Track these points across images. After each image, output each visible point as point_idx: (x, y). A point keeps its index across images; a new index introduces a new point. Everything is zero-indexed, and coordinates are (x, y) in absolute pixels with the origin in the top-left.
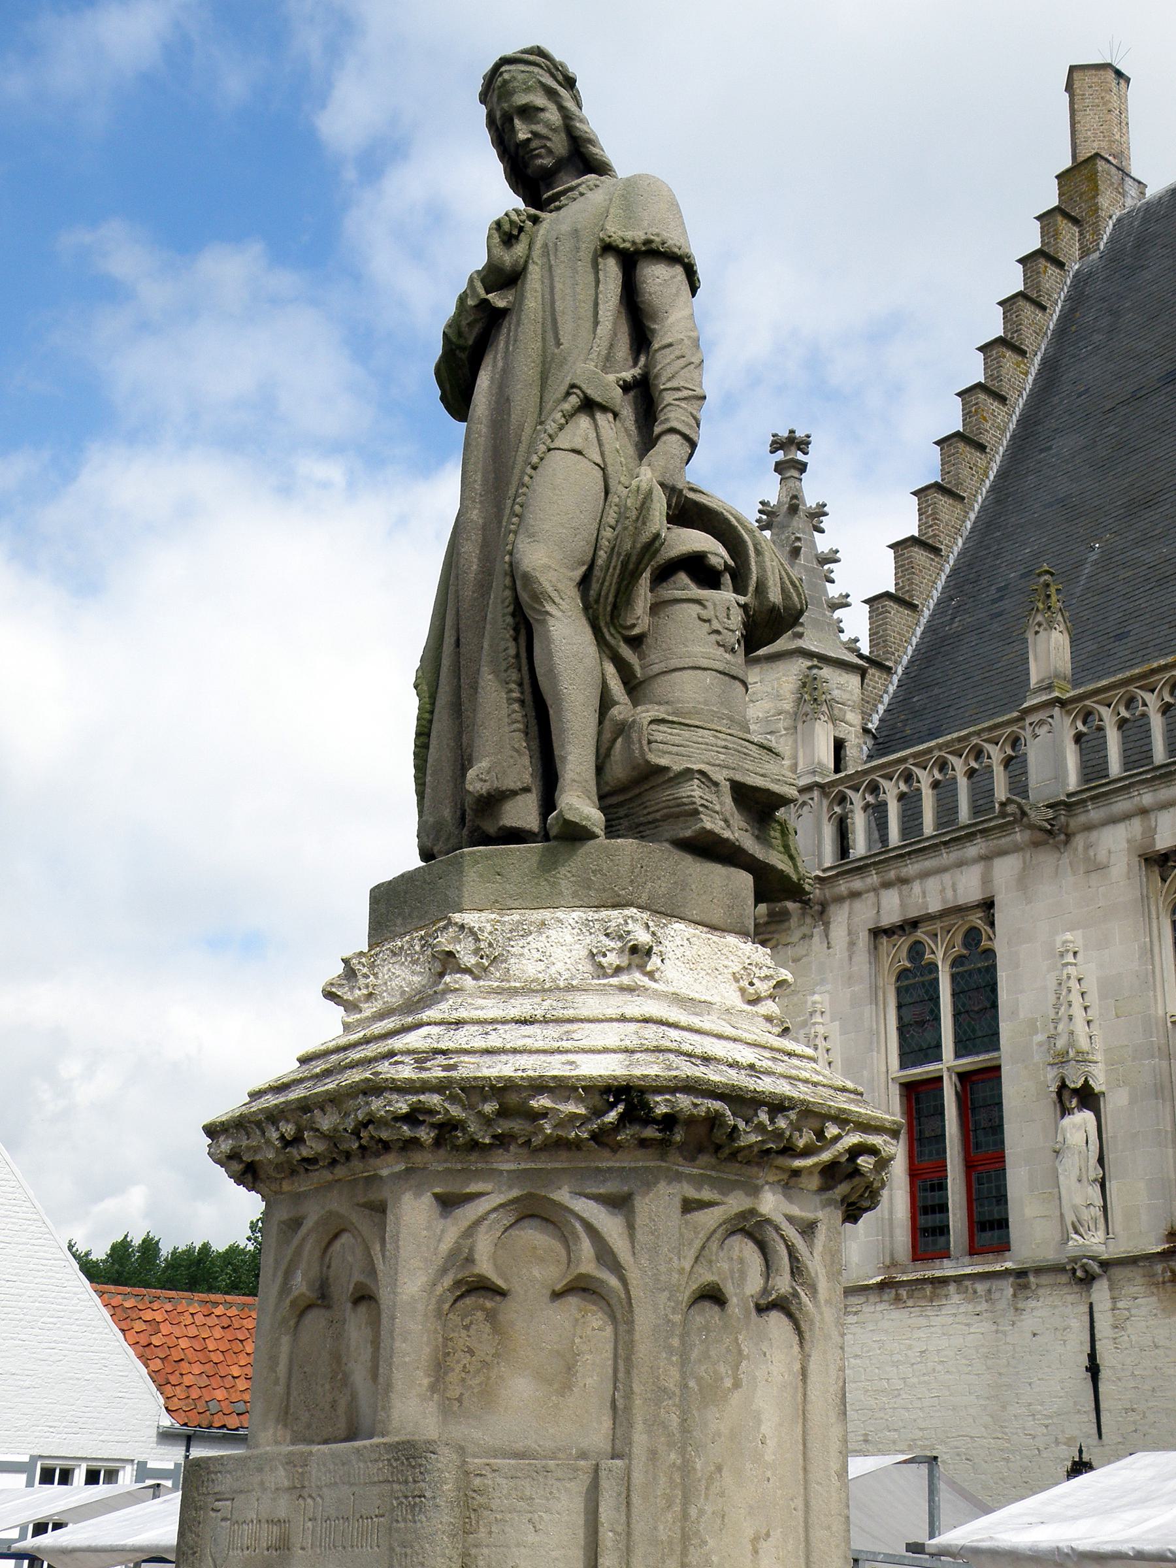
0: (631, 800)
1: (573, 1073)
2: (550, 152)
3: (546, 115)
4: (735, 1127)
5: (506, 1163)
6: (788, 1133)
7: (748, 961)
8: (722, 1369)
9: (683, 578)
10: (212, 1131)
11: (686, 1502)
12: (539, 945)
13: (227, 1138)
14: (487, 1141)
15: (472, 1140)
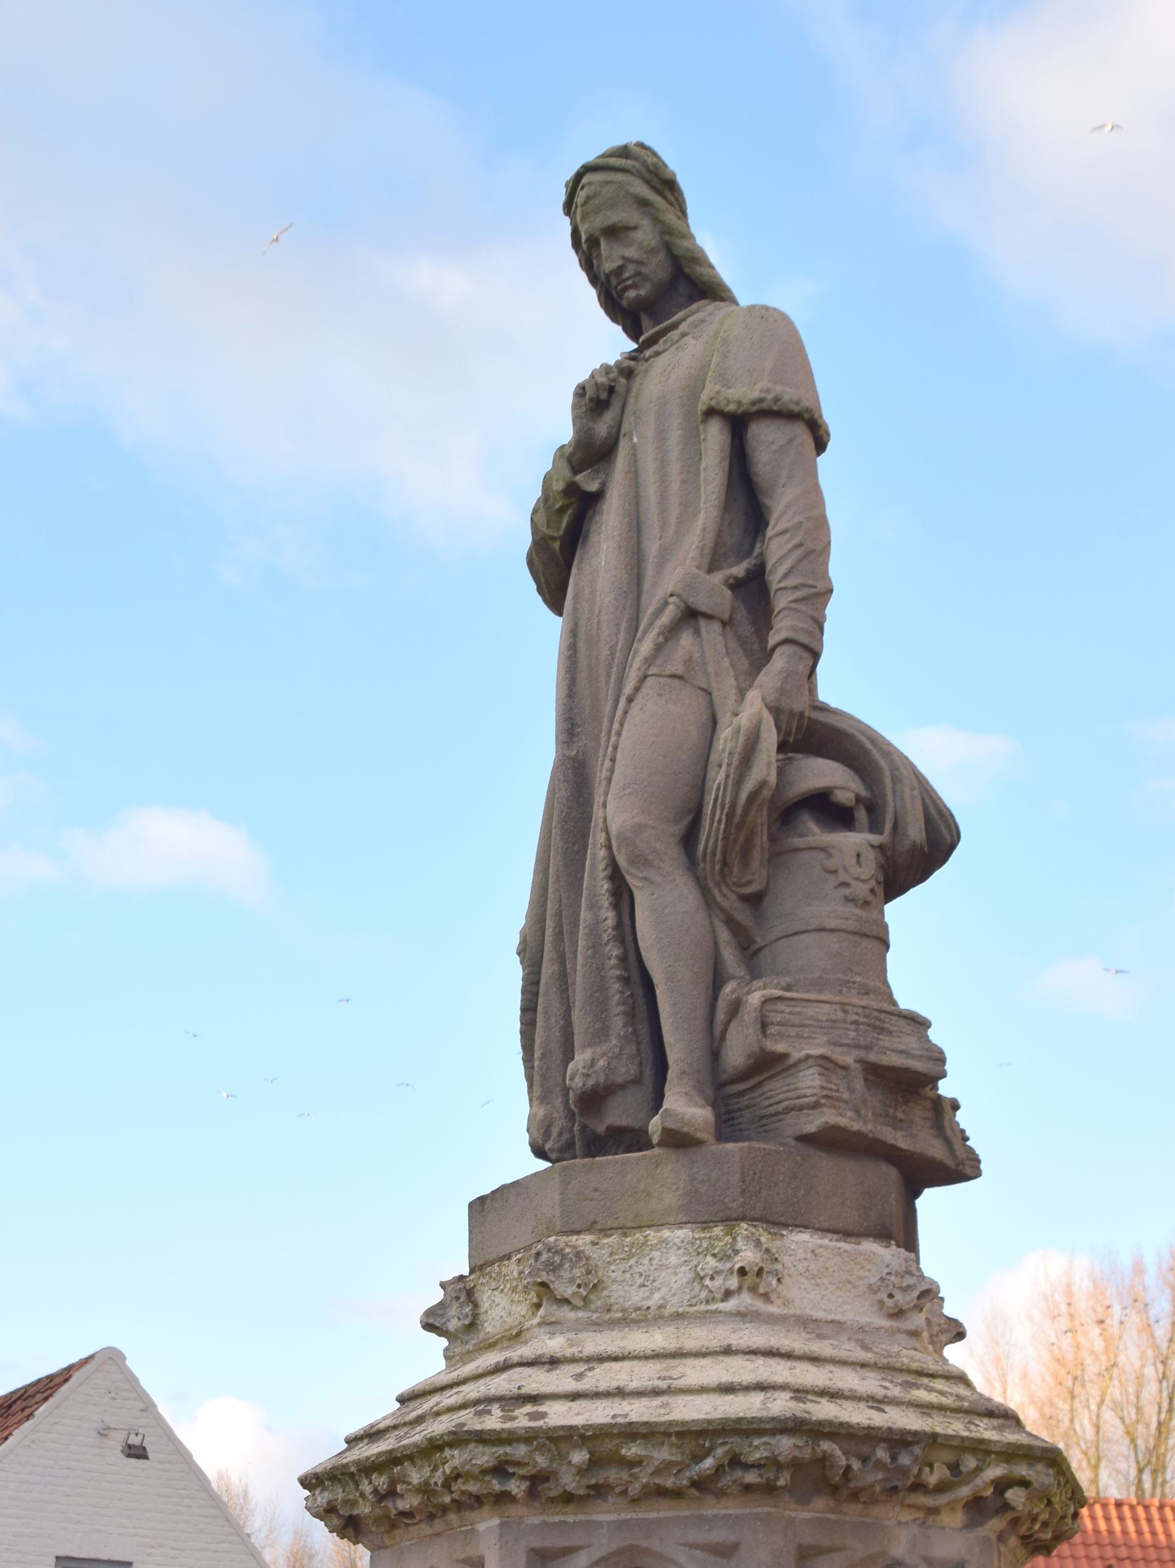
0: (752, 1089)
1: (666, 1418)
3: (639, 235)
4: (848, 1468)
5: (605, 1514)
6: (916, 1471)
7: (886, 1270)
10: (310, 1482)
12: (641, 1269)
13: (323, 1490)
14: (581, 1492)
15: (565, 1491)
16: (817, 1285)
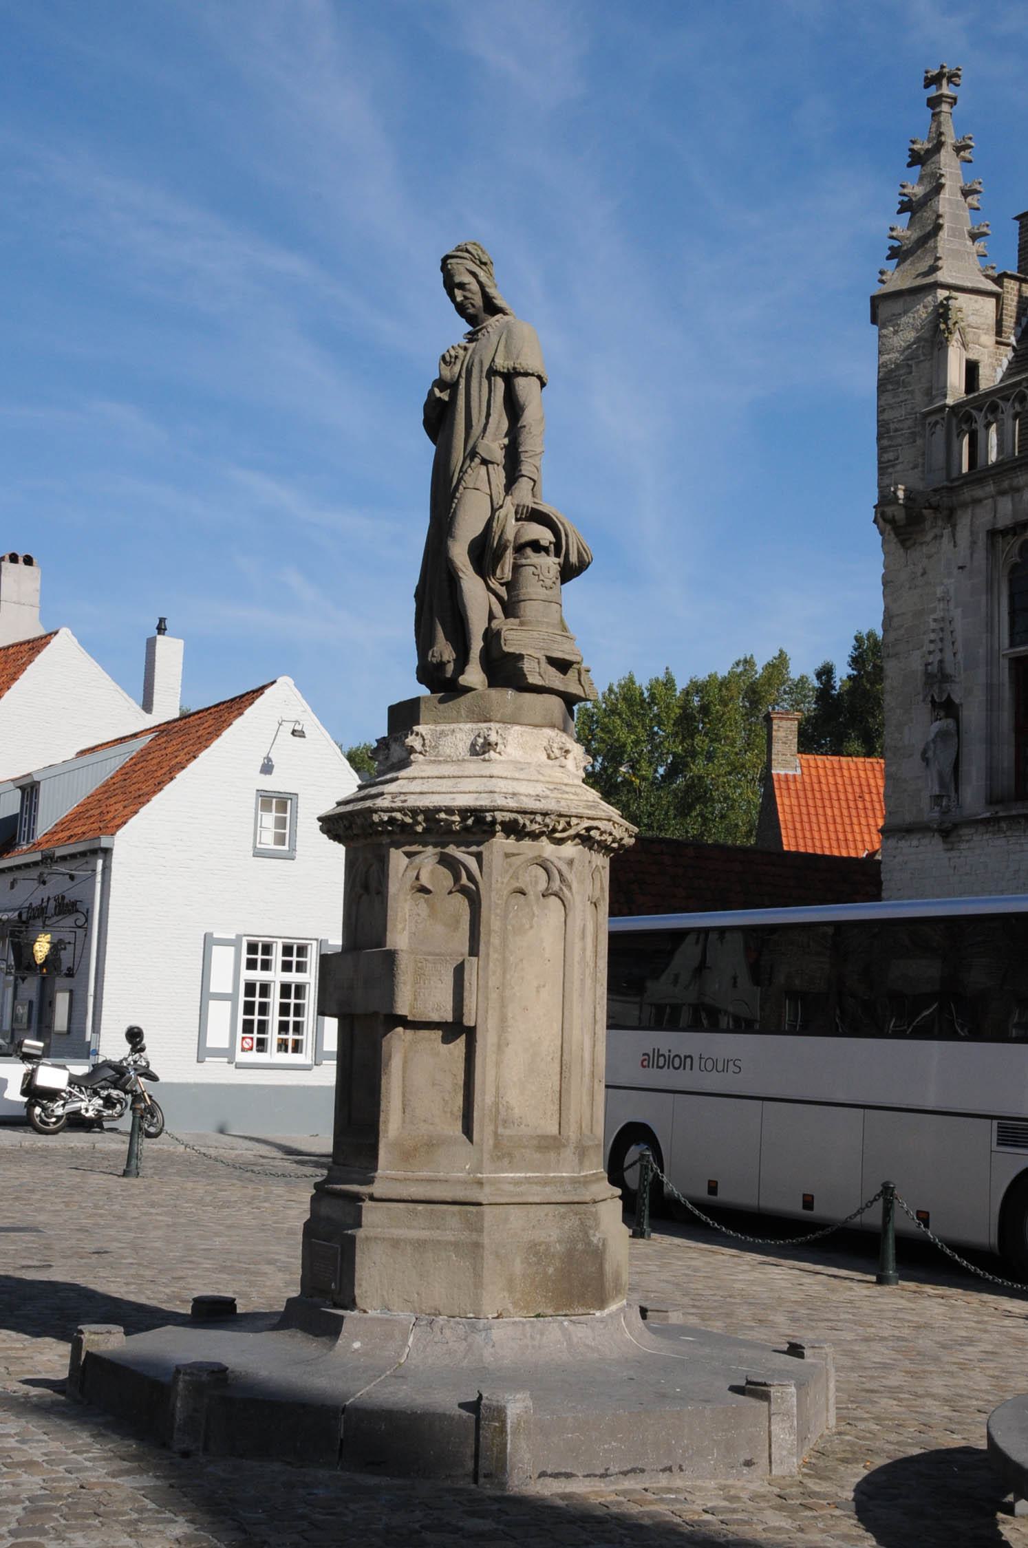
2: (473, 305)
8: (524, 921)
9: (529, 551)
11: (504, 973)
16: (609, 732)
